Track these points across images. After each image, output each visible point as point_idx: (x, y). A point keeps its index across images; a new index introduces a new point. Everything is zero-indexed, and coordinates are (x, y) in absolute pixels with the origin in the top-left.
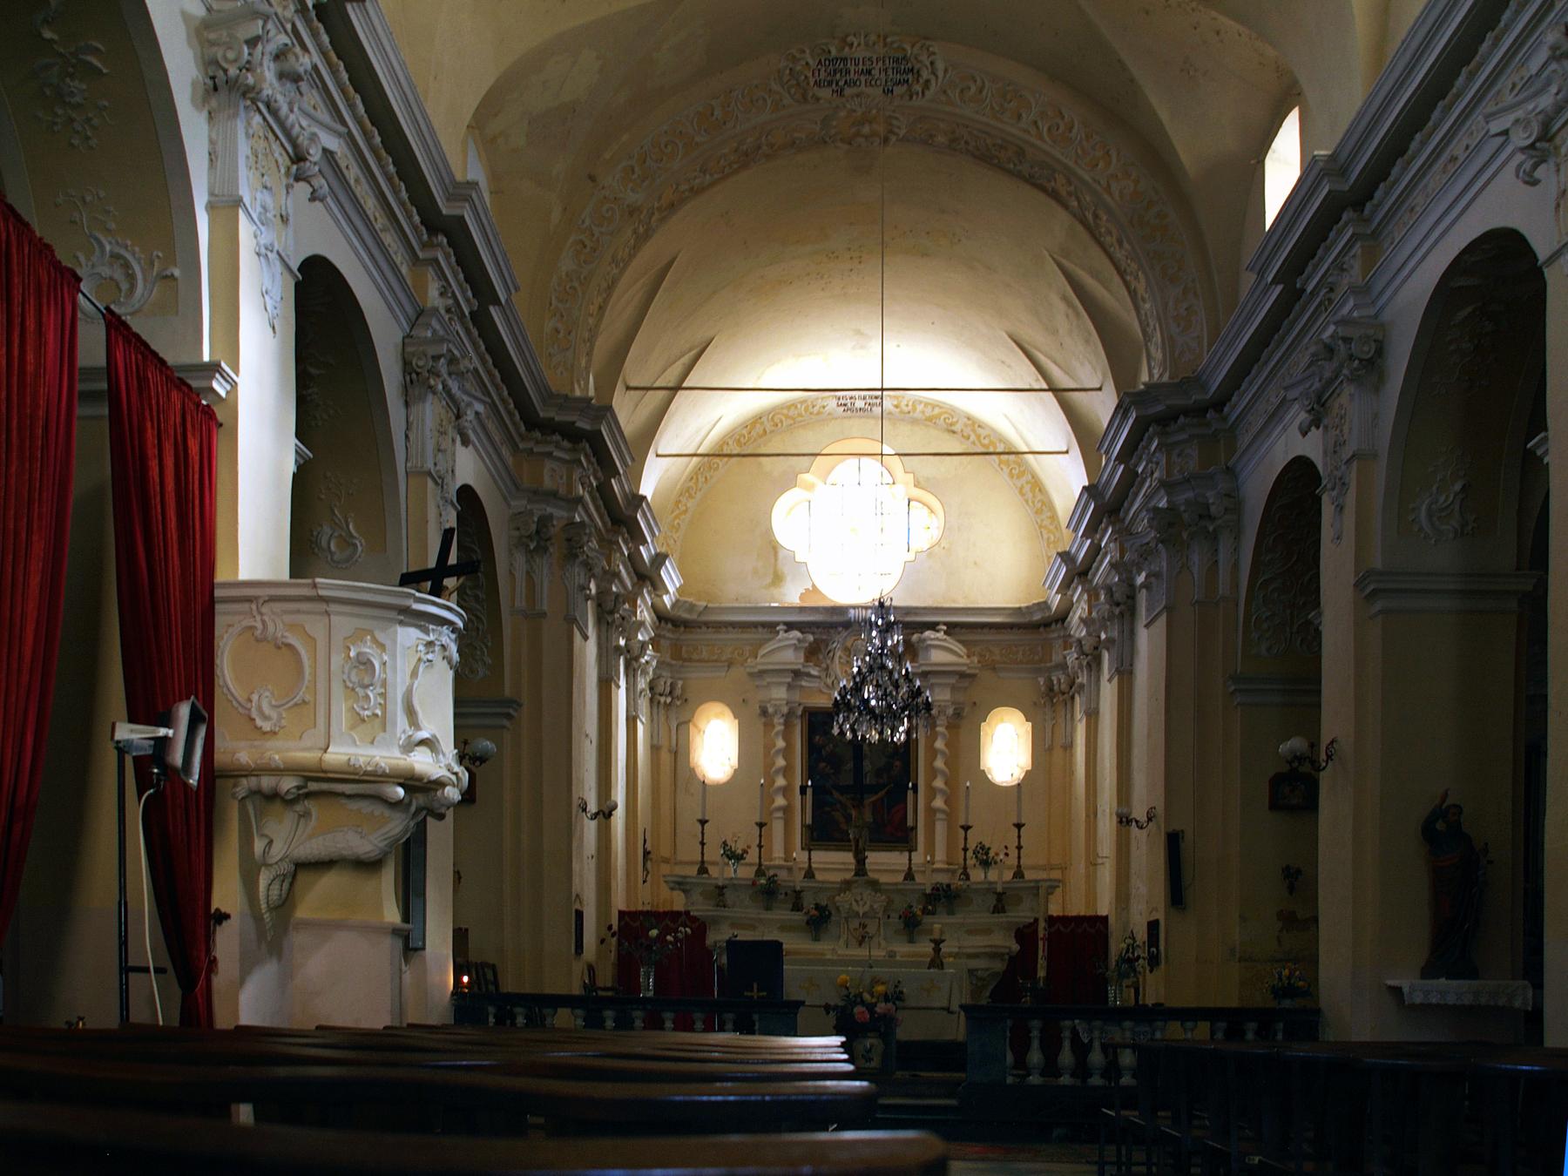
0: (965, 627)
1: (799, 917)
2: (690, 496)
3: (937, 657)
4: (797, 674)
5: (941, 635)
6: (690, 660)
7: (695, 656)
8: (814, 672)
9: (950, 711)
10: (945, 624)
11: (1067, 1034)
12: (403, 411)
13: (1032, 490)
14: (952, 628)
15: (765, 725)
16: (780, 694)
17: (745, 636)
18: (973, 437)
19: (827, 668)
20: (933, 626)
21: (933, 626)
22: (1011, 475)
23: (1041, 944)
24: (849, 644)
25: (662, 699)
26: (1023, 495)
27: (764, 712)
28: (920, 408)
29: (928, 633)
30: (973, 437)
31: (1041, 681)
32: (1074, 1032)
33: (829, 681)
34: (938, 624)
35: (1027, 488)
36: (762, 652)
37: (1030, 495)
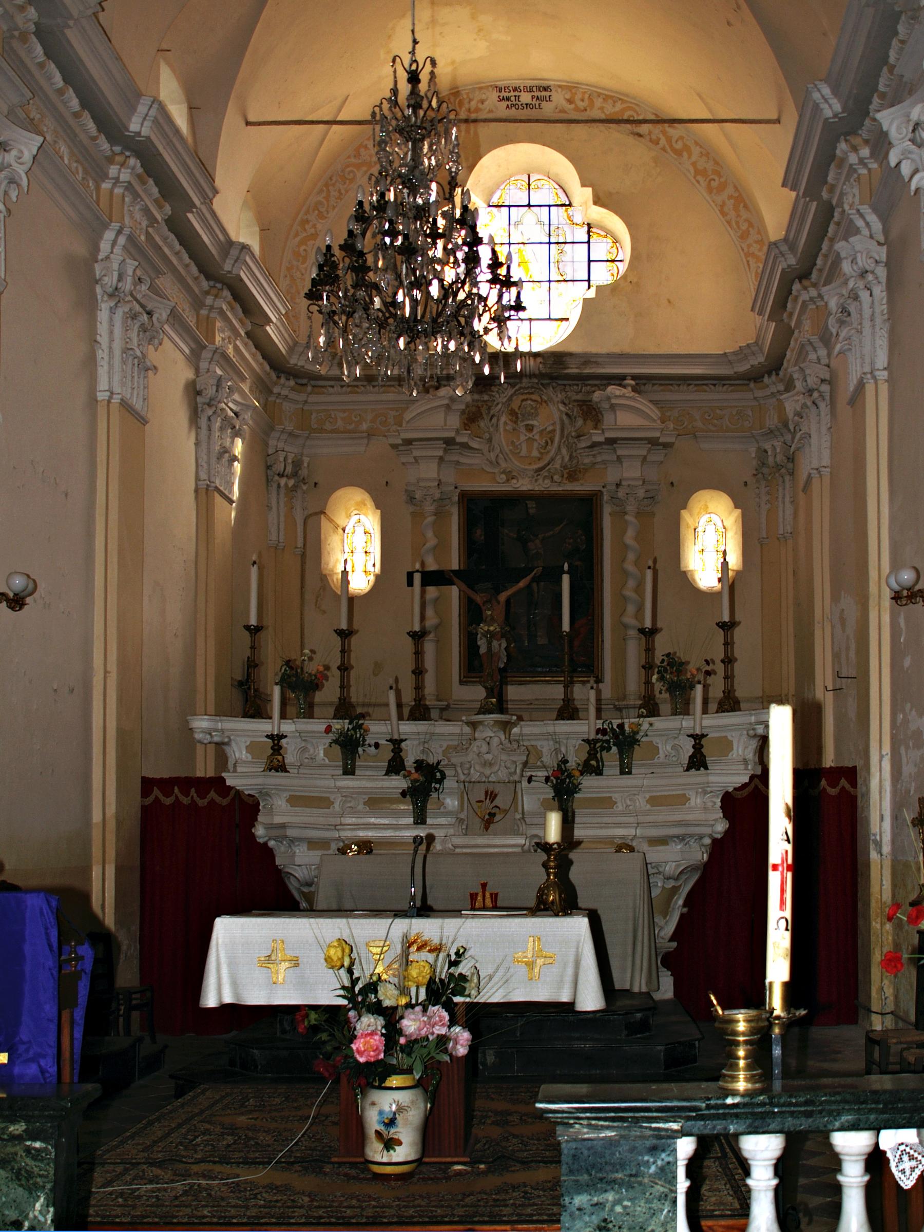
0: (653, 381)
1: (399, 783)
2: (321, 216)
3: (625, 419)
4: (449, 442)
5: (628, 392)
6: (322, 430)
7: (328, 426)
8: (474, 445)
9: (641, 493)
10: (634, 377)
11: (853, 1177)
12: (883, 812)
13: (736, 208)
14: (642, 382)
15: (413, 514)
16: (429, 471)
17: (384, 397)
18: (663, 141)
19: (490, 440)
20: (619, 379)
21: (619, 379)
22: (710, 190)
23: (774, 879)
24: (515, 405)
25: (283, 481)
26: (723, 214)
27: (411, 499)
28: (598, 102)
29: (612, 390)
30: (663, 141)
31: (753, 450)
32: (876, 1161)
33: (493, 456)
34: (623, 377)
35: (730, 203)
36: (408, 416)
37: (732, 214)
